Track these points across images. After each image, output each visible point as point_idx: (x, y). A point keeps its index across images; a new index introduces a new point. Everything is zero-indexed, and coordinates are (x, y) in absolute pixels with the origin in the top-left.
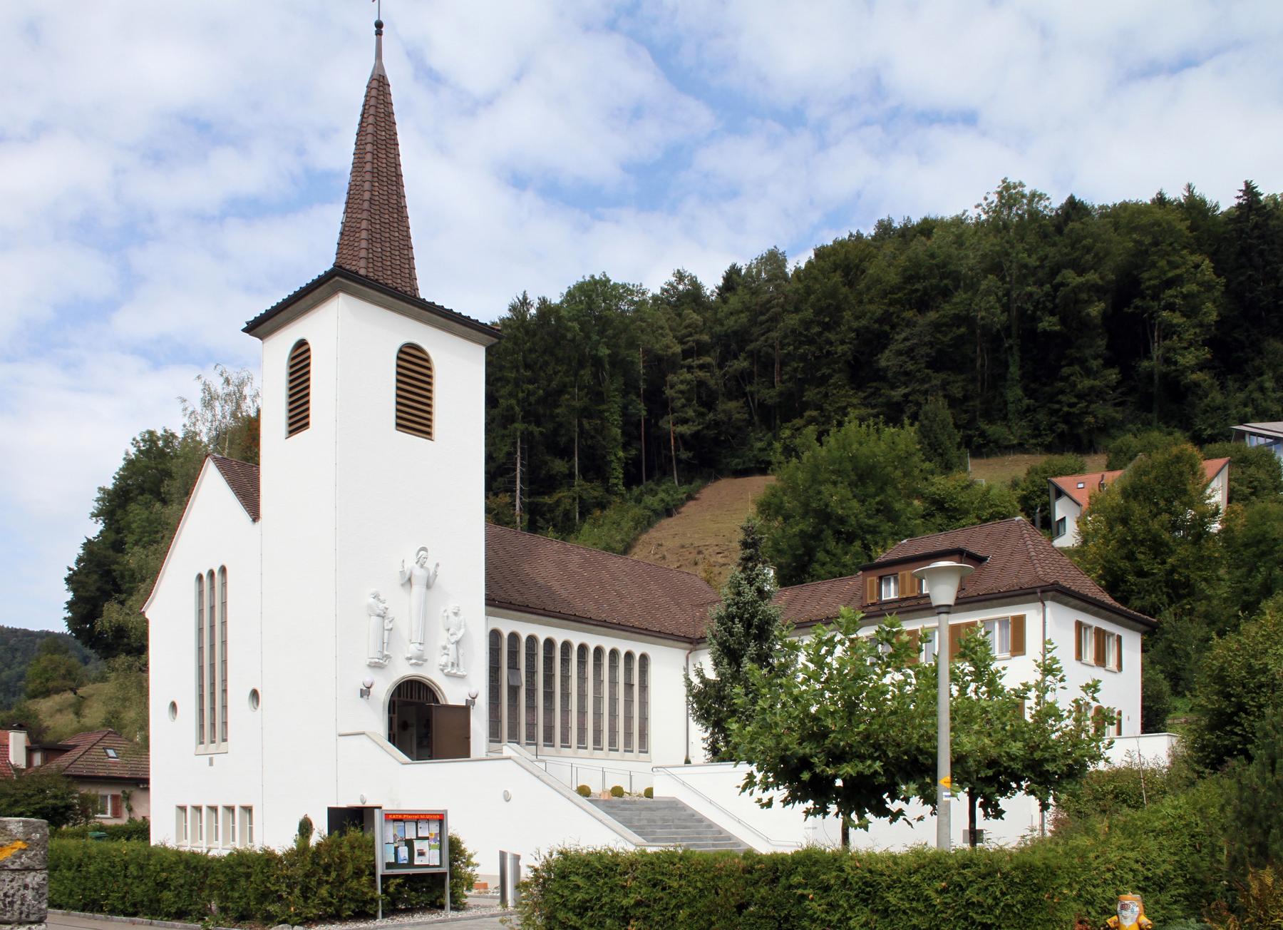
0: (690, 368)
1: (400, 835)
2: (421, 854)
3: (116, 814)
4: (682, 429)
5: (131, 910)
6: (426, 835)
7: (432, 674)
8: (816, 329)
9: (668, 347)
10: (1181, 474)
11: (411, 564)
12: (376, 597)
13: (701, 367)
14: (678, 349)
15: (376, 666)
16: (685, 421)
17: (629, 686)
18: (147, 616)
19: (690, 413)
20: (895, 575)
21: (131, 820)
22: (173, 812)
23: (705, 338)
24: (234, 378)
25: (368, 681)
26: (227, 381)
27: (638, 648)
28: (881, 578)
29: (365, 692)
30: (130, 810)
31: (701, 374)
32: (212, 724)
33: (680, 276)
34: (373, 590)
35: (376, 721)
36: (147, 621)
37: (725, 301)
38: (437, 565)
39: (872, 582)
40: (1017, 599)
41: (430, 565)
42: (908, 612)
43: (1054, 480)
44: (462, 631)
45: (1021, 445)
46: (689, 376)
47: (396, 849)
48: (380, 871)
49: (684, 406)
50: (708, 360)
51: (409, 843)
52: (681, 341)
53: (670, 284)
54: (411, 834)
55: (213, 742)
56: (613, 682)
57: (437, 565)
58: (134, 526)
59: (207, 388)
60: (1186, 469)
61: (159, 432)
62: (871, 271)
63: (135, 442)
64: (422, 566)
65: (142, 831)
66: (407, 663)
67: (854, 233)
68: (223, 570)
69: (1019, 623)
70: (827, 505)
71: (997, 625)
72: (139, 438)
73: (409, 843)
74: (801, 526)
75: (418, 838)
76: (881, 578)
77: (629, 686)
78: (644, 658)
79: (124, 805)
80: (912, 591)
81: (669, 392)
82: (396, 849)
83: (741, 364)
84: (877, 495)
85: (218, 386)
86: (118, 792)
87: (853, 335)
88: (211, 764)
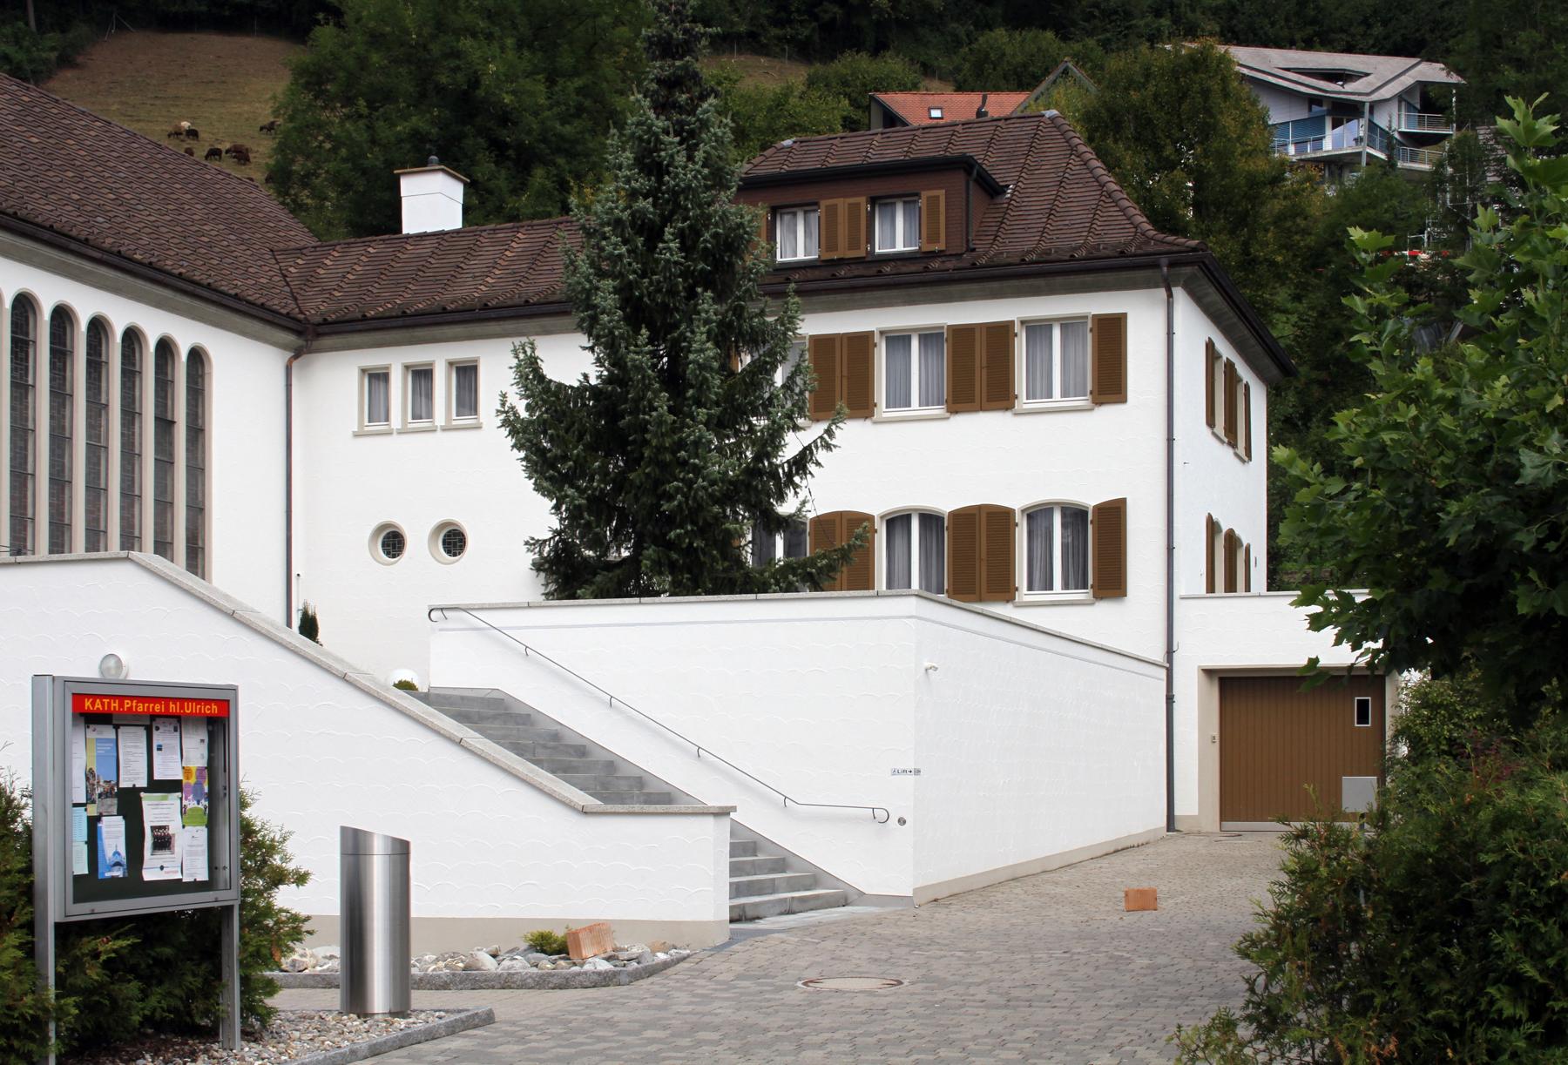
1: (105, 775)
2: (163, 842)
6: (178, 775)
10: (1206, 93)
17: (165, 424)
20: (909, 198)
27: (187, 334)
28: (775, 211)
39: (854, 208)
40: (1110, 277)
42: (854, 289)
43: (881, 97)
45: (753, 35)
47: (93, 822)
48: (56, 906)
51: (129, 804)
54: (133, 775)
56: (130, 414)
60: (1215, 85)
69: (1111, 333)
70: (475, 82)
71: (915, 344)
73: (129, 804)
74: (415, 121)
75: (157, 786)
76: (775, 211)
77: (165, 424)
80: (854, 244)
82: (93, 822)
84: (576, 73)
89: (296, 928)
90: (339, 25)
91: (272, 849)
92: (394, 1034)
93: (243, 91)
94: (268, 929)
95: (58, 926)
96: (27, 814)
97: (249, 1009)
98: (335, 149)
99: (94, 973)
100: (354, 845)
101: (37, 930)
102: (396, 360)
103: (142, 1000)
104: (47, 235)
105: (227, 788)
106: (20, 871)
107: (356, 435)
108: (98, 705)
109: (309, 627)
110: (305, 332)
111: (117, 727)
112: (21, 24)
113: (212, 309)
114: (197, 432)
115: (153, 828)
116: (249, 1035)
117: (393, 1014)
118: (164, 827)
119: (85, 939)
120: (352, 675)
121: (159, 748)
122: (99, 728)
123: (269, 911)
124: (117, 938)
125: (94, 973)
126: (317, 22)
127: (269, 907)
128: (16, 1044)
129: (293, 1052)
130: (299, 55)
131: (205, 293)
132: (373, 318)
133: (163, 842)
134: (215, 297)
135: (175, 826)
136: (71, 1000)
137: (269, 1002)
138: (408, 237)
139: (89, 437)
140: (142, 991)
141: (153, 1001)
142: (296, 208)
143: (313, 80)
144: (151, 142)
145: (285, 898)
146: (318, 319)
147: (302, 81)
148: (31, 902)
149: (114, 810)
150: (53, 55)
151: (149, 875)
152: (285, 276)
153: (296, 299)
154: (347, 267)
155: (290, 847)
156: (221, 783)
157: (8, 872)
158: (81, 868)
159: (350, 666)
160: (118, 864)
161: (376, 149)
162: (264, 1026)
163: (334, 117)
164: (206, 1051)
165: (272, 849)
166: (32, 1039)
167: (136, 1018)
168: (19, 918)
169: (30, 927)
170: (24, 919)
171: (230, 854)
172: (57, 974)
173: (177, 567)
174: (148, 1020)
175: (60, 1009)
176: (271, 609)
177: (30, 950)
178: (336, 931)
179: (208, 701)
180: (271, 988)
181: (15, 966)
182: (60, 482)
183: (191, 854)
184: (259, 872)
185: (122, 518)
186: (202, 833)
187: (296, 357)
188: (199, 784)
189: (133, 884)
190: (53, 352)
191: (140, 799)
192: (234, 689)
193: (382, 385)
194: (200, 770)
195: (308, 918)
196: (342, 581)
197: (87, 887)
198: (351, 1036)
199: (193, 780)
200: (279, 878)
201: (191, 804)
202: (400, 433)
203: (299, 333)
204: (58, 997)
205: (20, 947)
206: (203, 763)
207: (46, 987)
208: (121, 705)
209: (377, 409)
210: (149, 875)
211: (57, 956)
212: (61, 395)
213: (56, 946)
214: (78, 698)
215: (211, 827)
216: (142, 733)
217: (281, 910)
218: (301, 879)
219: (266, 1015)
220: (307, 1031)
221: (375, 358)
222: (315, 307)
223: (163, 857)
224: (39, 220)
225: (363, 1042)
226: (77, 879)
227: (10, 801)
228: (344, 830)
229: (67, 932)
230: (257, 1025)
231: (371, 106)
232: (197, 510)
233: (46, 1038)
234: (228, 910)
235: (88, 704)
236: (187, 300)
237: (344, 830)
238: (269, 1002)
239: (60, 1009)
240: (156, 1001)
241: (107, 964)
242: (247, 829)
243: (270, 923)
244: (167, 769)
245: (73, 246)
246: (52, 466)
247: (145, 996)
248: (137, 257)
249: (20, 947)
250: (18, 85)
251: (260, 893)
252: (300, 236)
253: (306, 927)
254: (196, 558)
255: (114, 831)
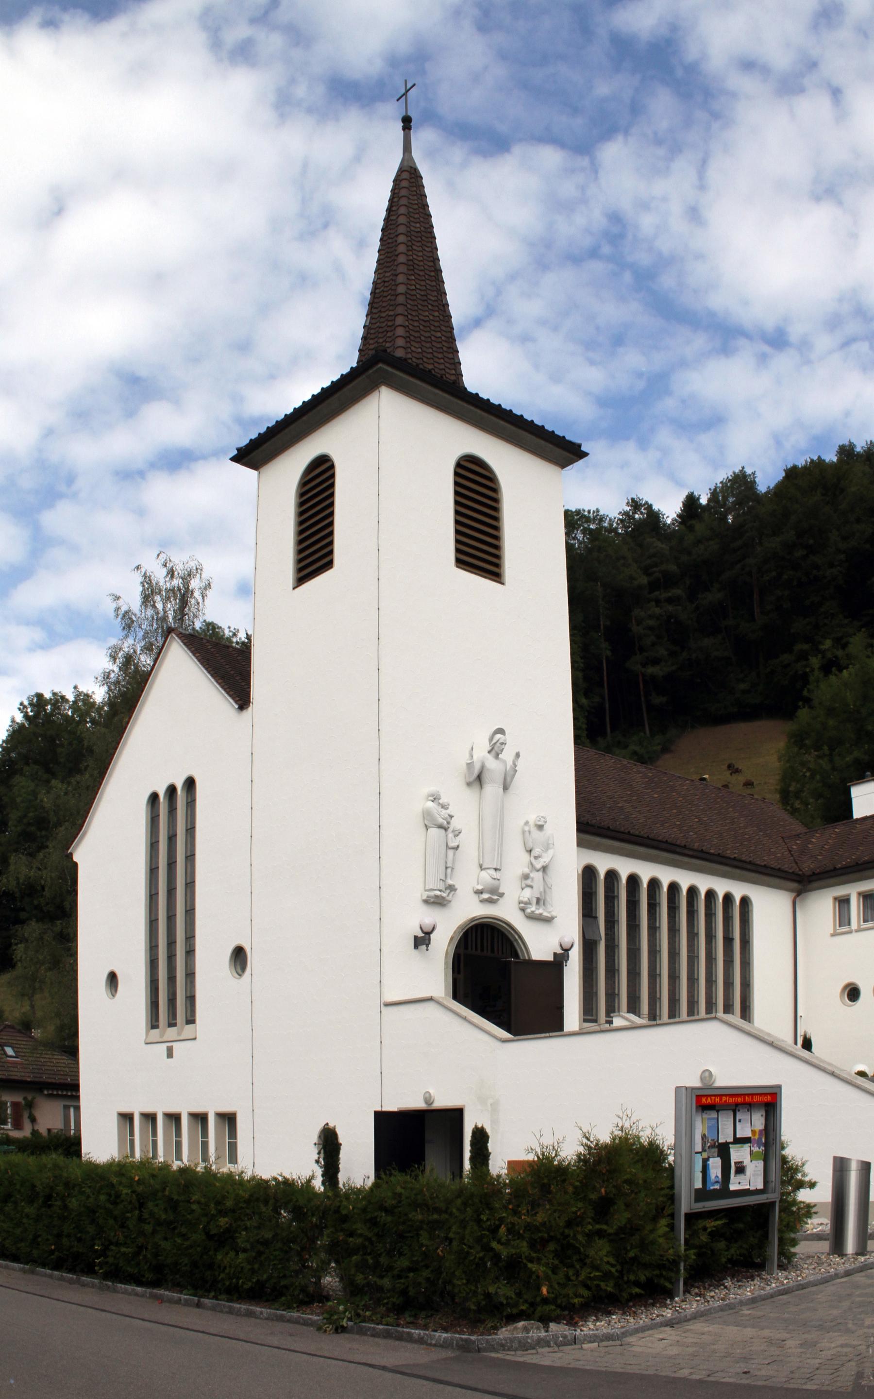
0: (658, 602)
1: (711, 1137)
3: (18, 1125)
4: (650, 670)
5: (149, 1276)
6: (749, 1134)
7: (507, 911)
8: (799, 553)
9: (632, 578)
11: (481, 753)
12: (435, 798)
13: (670, 601)
14: (644, 580)
15: (437, 902)
16: (655, 662)
17: (728, 940)
18: (75, 859)
19: (662, 652)
21: (35, 1133)
22: (113, 1124)
23: (673, 568)
24: (179, 569)
25: (428, 922)
26: (171, 573)
27: (738, 890)
29: (422, 940)
30: (33, 1120)
31: (670, 608)
32: (171, 1000)
33: (635, 504)
34: (432, 789)
35: (433, 974)
36: (76, 864)
37: (691, 529)
38: (518, 755)
41: (507, 755)
44: (551, 852)
46: (657, 611)
47: (705, 1162)
48: (686, 1204)
49: (653, 644)
50: (677, 592)
51: (723, 1151)
52: (646, 571)
53: (626, 513)
54: (725, 1136)
55: (172, 1024)
56: (710, 937)
57: (518, 755)
58: (18, 800)
59: (147, 579)
61: (48, 695)
62: (853, 489)
63: (22, 708)
64: (497, 756)
65: (71, 1145)
66: (475, 898)
67: (815, 458)
68: (190, 783)
72: (26, 703)
74: (856, 754)
75: (738, 1141)
77: (728, 940)
78: (745, 902)
79: (26, 1115)
81: (635, 629)
82: (705, 1162)
83: (713, 596)
85: (159, 575)
86: (18, 1098)
87: (842, 557)
88: (170, 1053)
89: (808, 1210)
90: (811, 707)
91: (796, 1170)
92: (858, 1265)
93: (762, 753)
94: (793, 1213)
95: (687, 1215)
96: (671, 1158)
97: (781, 1253)
98: (812, 777)
99: (704, 1238)
100: (841, 1166)
101: (676, 1216)
102: (853, 891)
103: (727, 1251)
104: (664, 846)
105: (775, 1139)
106: (668, 1188)
107: (832, 935)
108: (709, 1100)
109: (807, 1044)
110: (801, 881)
111: (718, 1111)
112: (642, 734)
113: (753, 875)
114: (746, 943)
115: (735, 1163)
116: (782, 1267)
117: (857, 1254)
118: (741, 1162)
119: (700, 1221)
120: (837, 1072)
121: (740, 1121)
122: (708, 1112)
123: (795, 1202)
124: (716, 1220)
125: (704, 1238)
126: (799, 707)
127: (795, 1200)
128: (664, 1273)
129: (804, 1275)
130: (789, 726)
131: (749, 867)
132: (841, 869)
133: (741, 1170)
134: (753, 868)
135: (747, 1161)
136: (692, 1251)
137: (793, 1250)
138: (857, 820)
139: (688, 951)
140: (727, 1246)
141: (732, 1251)
142: (794, 812)
143: (798, 740)
144: (715, 788)
145: (804, 1196)
146: (810, 873)
147: (793, 740)
148: (673, 1202)
149: (716, 1154)
150: (659, 747)
151: (733, 1187)
152: (790, 851)
153: (796, 863)
154: (823, 841)
155: (806, 1169)
156: (771, 1137)
157: (662, 1189)
158: (698, 1185)
159: (836, 1067)
160: (717, 1182)
161: (835, 773)
162: (789, 1262)
163: (810, 757)
164: (759, 1276)
165: (796, 1170)
166: (672, 1270)
167: (724, 1260)
168: (667, 1211)
169: (672, 1216)
170: (670, 1212)
171: (774, 1176)
172: (686, 1239)
173: (735, 1018)
174: (730, 1261)
175: (687, 1256)
176: (784, 1034)
177: (672, 1227)
178: (829, 1211)
179: (766, 1094)
180: (794, 1243)
181: (665, 1235)
182: (674, 977)
183: (754, 1175)
184: (789, 1182)
185: (706, 993)
186: (760, 1164)
187: (798, 895)
188: (760, 1139)
189: (725, 1192)
190: (669, 908)
191: (729, 1148)
192: (779, 1087)
193: (846, 906)
194: (760, 1131)
195: (815, 1206)
196: (826, 1017)
197: (702, 1195)
198: (835, 1266)
199: (757, 1137)
200: (800, 1185)
201: (755, 1149)
202: (856, 931)
203: (799, 882)
204: (685, 1250)
205: (667, 1226)
206: (762, 1127)
207: (680, 1245)
208: (721, 1099)
209: (843, 919)
210: (733, 1187)
211: (686, 1230)
212: (673, 930)
213: (685, 1225)
214: (699, 1098)
215: (766, 1161)
216: (731, 1113)
217: (801, 1202)
218: (812, 1185)
219: (790, 1257)
220: (811, 1264)
221: (841, 891)
222: (808, 866)
223: (740, 1177)
224: (660, 838)
225: (841, 1269)
226: (697, 1190)
227: (662, 1152)
228: (835, 1158)
229: (691, 1218)
230: (785, 1261)
231: (832, 749)
232: (747, 985)
233: (678, 1270)
234: (773, 1204)
235: (704, 1100)
236: (738, 871)
237: (835, 1158)
238: (793, 1250)
239: (687, 1256)
240: (734, 1251)
241: (710, 1234)
242: (784, 1160)
243: (794, 1209)
244: (744, 1131)
245: (678, 850)
246: (669, 969)
247: (728, 1249)
248: (712, 851)
249: (667, 1226)
250: (646, 768)
251: (789, 1194)
252: (799, 828)
253: (813, 1210)
254: (746, 1012)
255: (715, 1166)
